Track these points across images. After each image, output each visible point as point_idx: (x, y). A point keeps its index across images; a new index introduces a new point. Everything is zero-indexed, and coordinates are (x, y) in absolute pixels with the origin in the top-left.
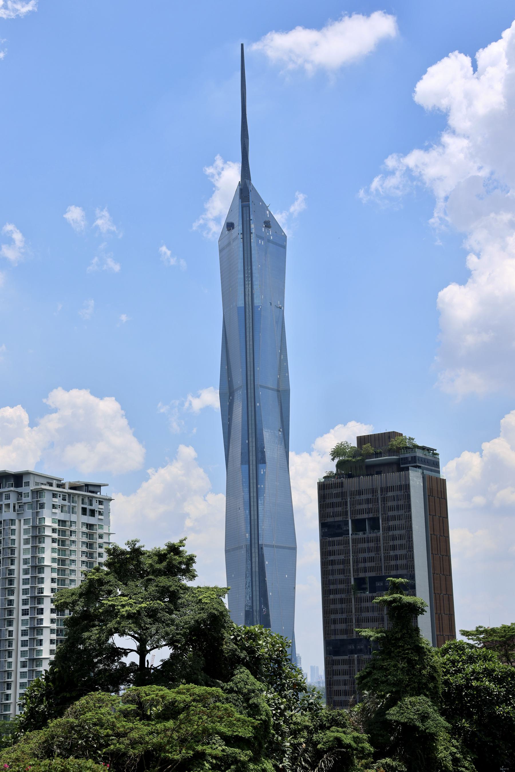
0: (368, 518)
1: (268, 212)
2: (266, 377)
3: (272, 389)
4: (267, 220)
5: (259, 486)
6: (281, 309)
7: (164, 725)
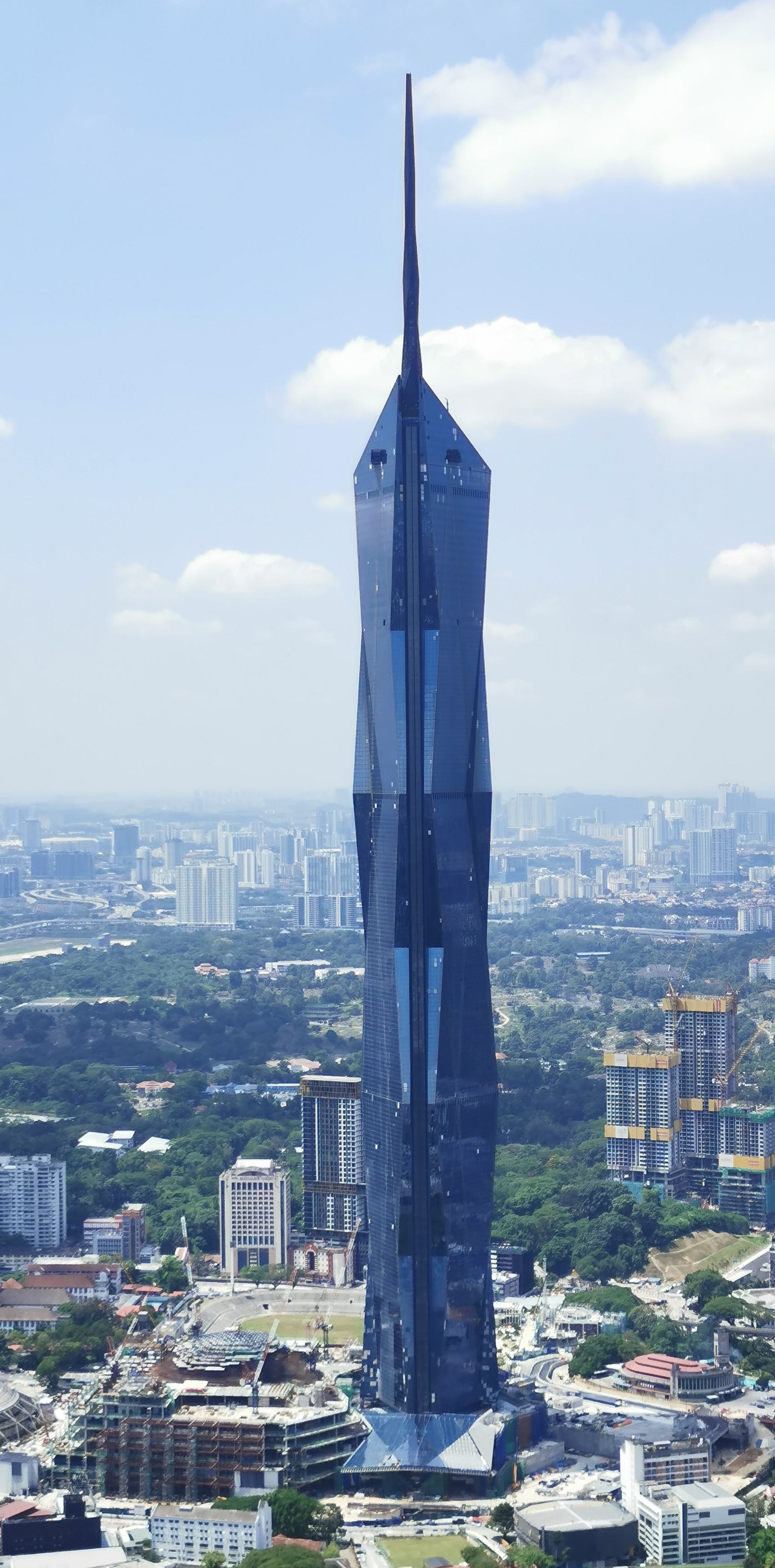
1: (454, 431)
5: (429, 991)
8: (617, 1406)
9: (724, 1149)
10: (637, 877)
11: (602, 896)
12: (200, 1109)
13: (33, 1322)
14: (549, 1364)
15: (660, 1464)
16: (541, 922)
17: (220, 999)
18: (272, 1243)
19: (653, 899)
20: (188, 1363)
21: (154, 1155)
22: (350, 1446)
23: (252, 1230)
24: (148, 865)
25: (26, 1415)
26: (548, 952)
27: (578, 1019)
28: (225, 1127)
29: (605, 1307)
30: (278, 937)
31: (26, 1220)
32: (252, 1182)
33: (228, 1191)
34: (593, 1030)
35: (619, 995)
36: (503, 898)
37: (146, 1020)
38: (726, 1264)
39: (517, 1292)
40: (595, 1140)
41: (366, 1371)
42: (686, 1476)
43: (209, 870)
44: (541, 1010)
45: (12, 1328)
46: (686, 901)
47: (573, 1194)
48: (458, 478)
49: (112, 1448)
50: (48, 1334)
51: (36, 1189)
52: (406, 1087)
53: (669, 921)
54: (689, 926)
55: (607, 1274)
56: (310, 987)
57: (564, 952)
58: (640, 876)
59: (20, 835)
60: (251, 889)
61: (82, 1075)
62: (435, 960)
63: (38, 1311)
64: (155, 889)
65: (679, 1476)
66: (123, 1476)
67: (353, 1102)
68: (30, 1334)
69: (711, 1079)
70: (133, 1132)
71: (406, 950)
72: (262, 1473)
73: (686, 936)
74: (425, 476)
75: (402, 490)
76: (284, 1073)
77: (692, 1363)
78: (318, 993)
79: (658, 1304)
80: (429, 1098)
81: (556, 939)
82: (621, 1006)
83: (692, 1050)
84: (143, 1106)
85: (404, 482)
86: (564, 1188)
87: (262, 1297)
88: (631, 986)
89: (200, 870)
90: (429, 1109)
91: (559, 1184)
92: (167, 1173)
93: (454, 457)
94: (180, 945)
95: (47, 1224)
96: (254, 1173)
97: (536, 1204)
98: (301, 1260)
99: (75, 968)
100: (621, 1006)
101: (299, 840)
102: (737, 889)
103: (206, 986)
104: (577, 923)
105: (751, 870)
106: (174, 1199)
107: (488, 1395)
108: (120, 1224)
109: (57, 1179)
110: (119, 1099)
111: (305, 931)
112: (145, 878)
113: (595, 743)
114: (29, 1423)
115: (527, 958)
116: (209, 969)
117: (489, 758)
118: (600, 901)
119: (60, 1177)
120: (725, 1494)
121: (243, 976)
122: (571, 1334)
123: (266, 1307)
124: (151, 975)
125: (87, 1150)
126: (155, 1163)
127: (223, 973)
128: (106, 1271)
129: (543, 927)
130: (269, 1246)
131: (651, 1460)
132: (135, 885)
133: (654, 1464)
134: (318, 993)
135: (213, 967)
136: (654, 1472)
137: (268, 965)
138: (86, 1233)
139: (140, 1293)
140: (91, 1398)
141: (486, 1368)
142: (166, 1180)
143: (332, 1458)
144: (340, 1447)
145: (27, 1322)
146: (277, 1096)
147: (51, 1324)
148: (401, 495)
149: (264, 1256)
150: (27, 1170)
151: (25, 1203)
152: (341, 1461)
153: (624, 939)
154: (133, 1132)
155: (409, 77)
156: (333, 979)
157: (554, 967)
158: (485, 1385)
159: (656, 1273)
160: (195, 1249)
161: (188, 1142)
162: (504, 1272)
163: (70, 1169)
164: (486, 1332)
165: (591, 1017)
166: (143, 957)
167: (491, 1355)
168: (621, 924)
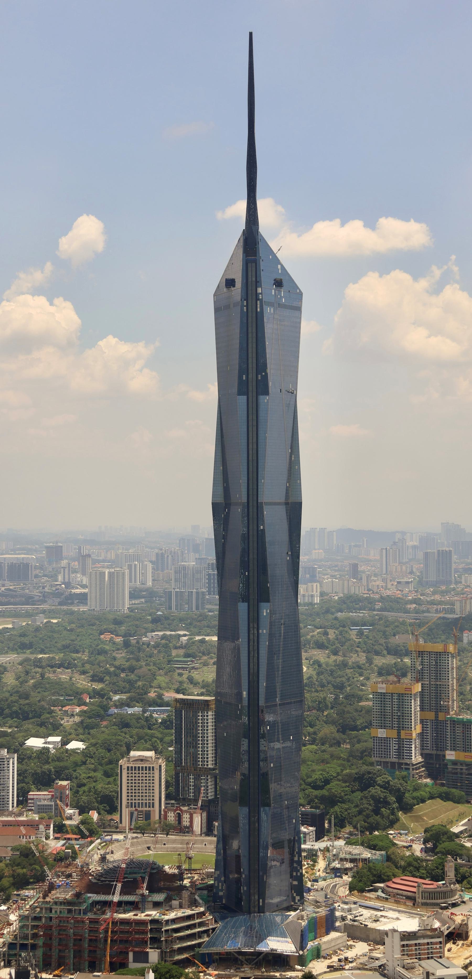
0: (398, 763)
1: (279, 266)
2: (271, 491)
3: (279, 504)
4: (279, 277)
5: (260, 631)
6: (293, 393)
7: (116, 628)
8: (381, 910)
9: (449, 748)
10: (388, 581)
11: (367, 592)
12: (105, 723)
15: (411, 945)
16: (327, 608)
17: (117, 655)
18: (153, 807)
19: (399, 594)
20: (99, 880)
23: (140, 798)
24: (69, 572)
26: (332, 627)
27: (351, 669)
29: (373, 847)
30: (155, 616)
32: (141, 766)
33: (125, 773)
34: (361, 675)
35: (377, 653)
36: (309, 592)
37: (68, 669)
38: (451, 823)
39: (314, 839)
40: (365, 743)
41: (216, 885)
42: (428, 953)
43: (109, 573)
44: (327, 664)
46: (421, 595)
47: (349, 775)
48: (281, 297)
49: (48, 936)
50: (5, 864)
53: (410, 608)
54: (423, 612)
55: (371, 829)
56: (176, 648)
57: (341, 626)
61: (27, 701)
62: (265, 611)
65: (424, 954)
66: (55, 954)
67: (207, 713)
69: (440, 701)
70: (60, 738)
71: (246, 604)
72: (148, 952)
73: (421, 618)
74: (260, 295)
75: (245, 304)
76: (159, 701)
77: (430, 882)
80: (260, 702)
81: (336, 619)
82: (379, 661)
84: (67, 723)
87: (146, 842)
89: (105, 573)
91: (341, 770)
92: (84, 763)
93: (279, 284)
95: (3, 796)
96: (142, 760)
97: (327, 782)
98: (171, 817)
99: (20, 636)
100: (379, 661)
101: (168, 556)
102: (454, 589)
103: (107, 648)
104: (350, 610)
106: (88, 780)
107: (297, 901)
108: (52, 795)
110: (51, 717)
111: (172, 613)
112: (67, 580)
113: (358, 504)
115: (318, 631)
116: (109, 637)
117: (300, 480)
118: (365, 596)
120: (455, 966)
121: (132, 641)
125: (30, 748)
126: (75, 756)
127: (119, 640)
129: (327, 611)
130: (151, 809)
131: (405, 943)
132: (61, 585)
133: (407, 945)
134: (181, 652)
135: (112, 636)
136: (408, 951)
137: (149, 634)
138: (30, 801)
140: (34, 903)
141: (295, 883)
143: (193, 943)
144: (200, 935)
146: (155, 715)
147: (7, 858)
148: (245, 308)
149: (148, 816)
152: (199, 945)
153: (380, 619)
154: (60, 738)
156: (191, 643)
157: (336, 636)
158: (295, 895)
159: (405, 828)
160: (102, 812)
161: (97, 744)
164: (296, 859)
165: (360, 667)
167: (299, 874)
168: (378, 610)
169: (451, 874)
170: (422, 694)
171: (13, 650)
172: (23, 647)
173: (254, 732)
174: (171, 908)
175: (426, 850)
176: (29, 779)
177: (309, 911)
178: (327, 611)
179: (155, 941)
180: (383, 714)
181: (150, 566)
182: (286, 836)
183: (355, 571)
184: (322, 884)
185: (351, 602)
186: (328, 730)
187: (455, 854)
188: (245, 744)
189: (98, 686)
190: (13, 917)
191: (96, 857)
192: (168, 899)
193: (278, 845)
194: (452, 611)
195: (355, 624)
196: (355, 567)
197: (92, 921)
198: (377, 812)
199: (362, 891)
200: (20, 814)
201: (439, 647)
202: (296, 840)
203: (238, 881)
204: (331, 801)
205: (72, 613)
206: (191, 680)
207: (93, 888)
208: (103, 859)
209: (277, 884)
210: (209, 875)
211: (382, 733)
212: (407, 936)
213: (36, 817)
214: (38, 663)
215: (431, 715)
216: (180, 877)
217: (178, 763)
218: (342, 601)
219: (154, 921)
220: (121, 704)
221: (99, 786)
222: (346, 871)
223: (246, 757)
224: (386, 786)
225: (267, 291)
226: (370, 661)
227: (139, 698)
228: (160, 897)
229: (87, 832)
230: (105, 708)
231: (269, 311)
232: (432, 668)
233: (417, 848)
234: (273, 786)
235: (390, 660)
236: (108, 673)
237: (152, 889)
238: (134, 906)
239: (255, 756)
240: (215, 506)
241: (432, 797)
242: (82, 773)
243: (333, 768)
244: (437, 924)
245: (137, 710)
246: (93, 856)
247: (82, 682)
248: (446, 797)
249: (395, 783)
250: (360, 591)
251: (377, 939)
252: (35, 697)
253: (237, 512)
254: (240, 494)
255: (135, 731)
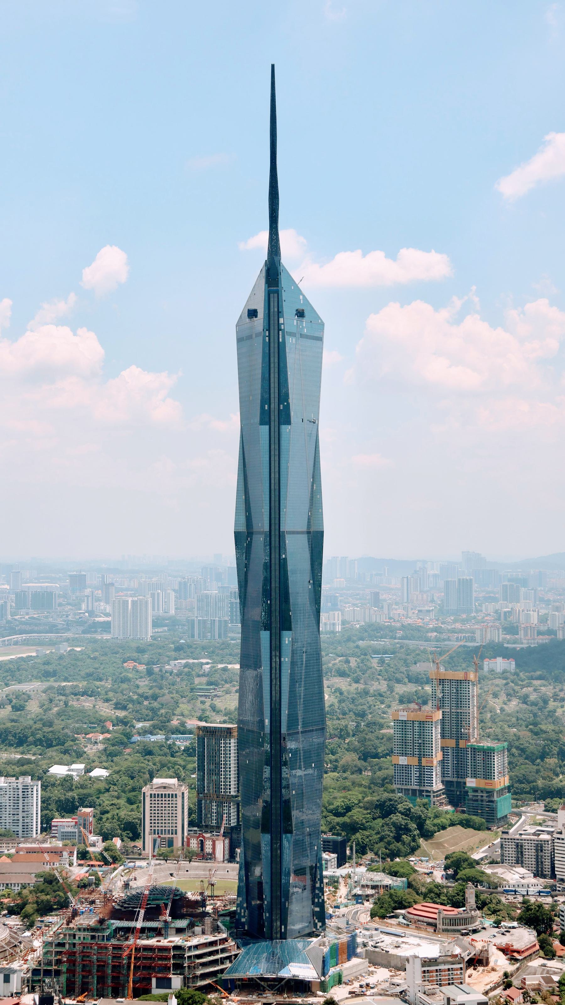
1: (301, 297)
2: (293, 520)
5: (282, 659)
8: (402, 937)
9: (470, 775)
10: (410, 609)
12: (128, 751)
13: (18, 884)
14: (357, 912)
17: (140, 683)
18: (176, 834)
19: (420, 623)
20: (122, 906)
21: (98, 779)
22: (228, 961)
24: (93, 600)
25: (13, 943)
26: (353, 655)
27: (373, 696)
28: (144, 761)
29: (394, 874)
30: (178, 645)
31: (13, 820)
32: (164, 793)
33: (148, 800)
34: (382, 703)
35: (398, 681)
36: (331, 620)
41: (239, 911)
42: (449, 979)
45: (4, 888)
46: (442, 624)
47: (371, 803)
49: (72, 963)
51: (21, 799)
52: (267, 722)
53: (431, 637)
55: (393, 855)
56: (199, 676)
58: (412, 609)
59: (8, 583)
60: (159, 616)
61: (51, 729)
62: (287, 639)
63: (24, 875)
64: (96, 616)
65: (445, 980)
66: (78, 980)
68: (16, 891)
71: (268, 632)
72: (171, 978)
74: (282, 326)
75: (267, 334)
76: (182, 729)
78: (204, 680)
79: (428, 874)
82: (400, 689)
83: (449, 710)
84: (91, 750)
85: (269, 330)
86: (366, 799)
88: (408, 677)
89: (128, 601)
90: (282, 736)
93: (300, 314)
94: (114, 649)
98: (194, 844)
99: (44, 664)
100: (400, 689)
101: (190, 585)
105: (484, 606)
106: (111, 807)
107: (318, 927)
109: (35, 792)
110: (75, 744)
112: (90, 609)
114: (15, 949)
115: (340, 659)
118: (386, 624)
119: (37, 791)
121: (155, 669)
122: (370, 892)
123: (171, 875)
124: (95, 669)
127: (142, 668)
128: (67, 851)
129: (349, 640)
130: (174, 836)
131: (426, 969)
132: (84, 613)
134: (204, 680)
135: (135, 664)
137: (172, 663)
138: (53, 828)
139: (89, 865)
140: (58, 929)
142: (106, 794)
145: (15, 884)
148: (267, 338)
150: (15, 786)
151: (13, 809)
152: (222, 971)
153: (402, 647)
155: (273, 66)
156: (213, 671)
159: (425, 854)
160: (125, 839)
161: (120, 771)
162: (327, 853)
163: (44, 787)
165: (381, 695)
166: (89, 657)
167: (320, 901)
169: (471, 900)
170: (443, 721)
171: (37, 678)
172: (47, 675)
173: (276, 760)
174: (194, 934)
175: (447, 877)
176: (53, 806)
177: (331, 938)
178: (349, 640)
179: (179, 968)
180: (404, 742)
181: (173, 595)
182: (308, 862)
183: (376, 600)
184: (343, 910)
185: (373, 630)
186: (349, 758)
187: (476, 881)
188: (267, 772)
189: (121, 714)
190: (37, 944)
191: (120, 884)
192: (191, 925)
193: (300, 872)
194: (473, 639)
195: (376, 652)
196: (376, 595)
197: (116, 947)
198: (398, 838)
199: (383, 917)
200: (44, 841)
201: (460, 676)
202: (315, 872)
203: (260, 907)
204: (353, 828)
205: (96, 641)
206: (213, 708)
207: (116, 914)
208: (126, 885)
209: (299, 910)
210: (232, 902)
211: (403, 761)
212: (427, 962)
213: (60, 844)
214: (61, 691)
215: (452, 743)
216: (203, 903)
217: (200, 790)
218: (364, 629)
219: (176, 948)
220: (144, 732)
221: (123, 813)
222: (367, 897)
223: (268, 785)
224: (407, 813)
225: (289, 321)
226: (391, 689)
227: (162, 726)
228: (182, 923)
229: (110, 859)
230: (128, 736)
231: (290, 341)
232: (453, 695)
233: (438, 876)
234: (295, 813)
235: (411, 688)
236: (131, 701)
237: (175, 915)
238: (158, 932)
239: (277, 784)
240: (237, 535)
241: (452, 824)
242: (106, 800)
243: (355, 795)
244: (457, 951)
245: (159, 737)
246: (116, 883)
247: (106, 710)
248: (466, 824)
249: (416, 810)
250: (381, 619)
251: (399, 966)
252: (58, 724)
253: (259, 541)
254: (262, 523)
255: (157, 759)
